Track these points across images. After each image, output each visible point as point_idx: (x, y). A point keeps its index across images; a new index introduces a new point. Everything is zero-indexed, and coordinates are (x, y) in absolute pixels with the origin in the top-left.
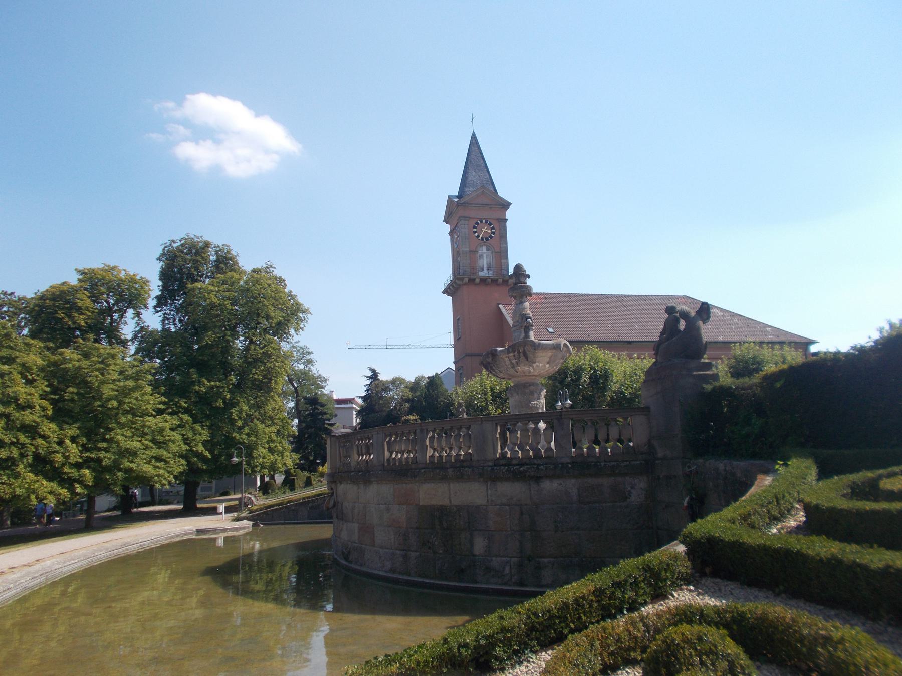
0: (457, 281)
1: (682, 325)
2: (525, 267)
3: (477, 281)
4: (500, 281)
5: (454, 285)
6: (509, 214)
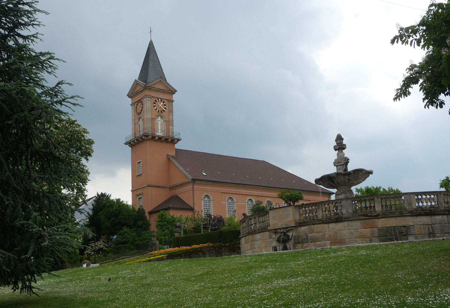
3: (157, 138)
6: (175, 97)
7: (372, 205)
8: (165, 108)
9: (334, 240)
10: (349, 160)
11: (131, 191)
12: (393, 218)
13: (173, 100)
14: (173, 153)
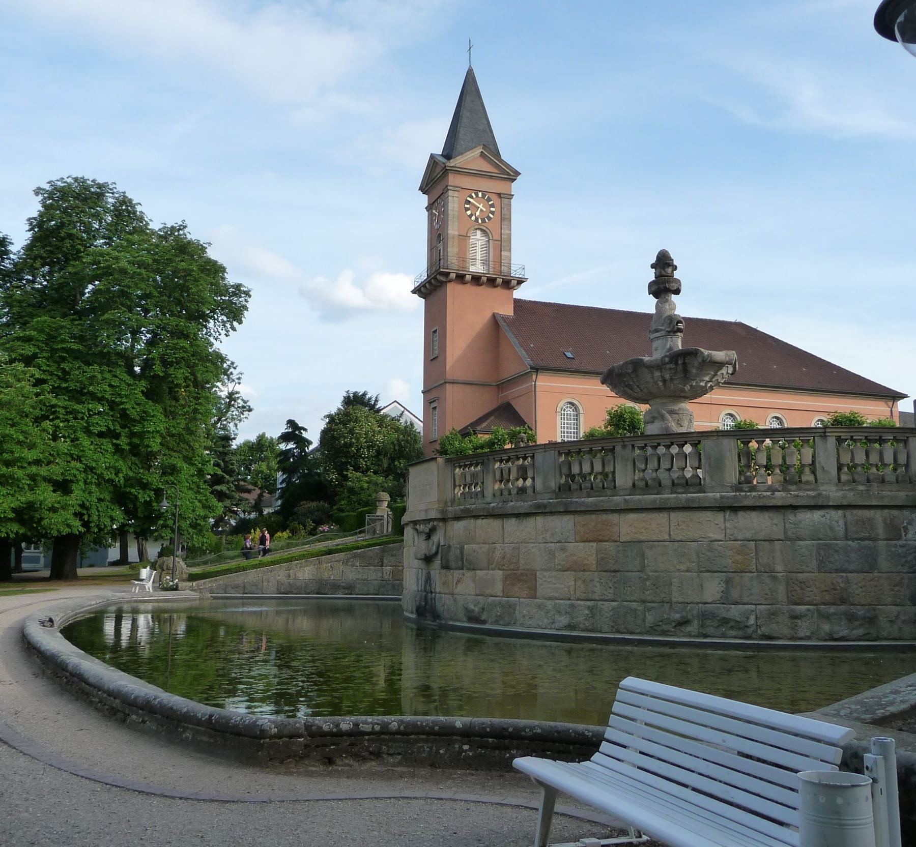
0: (438, 277)
3: (468, 277)
4: (499, 281)
5: (433, 281)
8: (493, 213)
9: (511, 570)
13: (512, 193)
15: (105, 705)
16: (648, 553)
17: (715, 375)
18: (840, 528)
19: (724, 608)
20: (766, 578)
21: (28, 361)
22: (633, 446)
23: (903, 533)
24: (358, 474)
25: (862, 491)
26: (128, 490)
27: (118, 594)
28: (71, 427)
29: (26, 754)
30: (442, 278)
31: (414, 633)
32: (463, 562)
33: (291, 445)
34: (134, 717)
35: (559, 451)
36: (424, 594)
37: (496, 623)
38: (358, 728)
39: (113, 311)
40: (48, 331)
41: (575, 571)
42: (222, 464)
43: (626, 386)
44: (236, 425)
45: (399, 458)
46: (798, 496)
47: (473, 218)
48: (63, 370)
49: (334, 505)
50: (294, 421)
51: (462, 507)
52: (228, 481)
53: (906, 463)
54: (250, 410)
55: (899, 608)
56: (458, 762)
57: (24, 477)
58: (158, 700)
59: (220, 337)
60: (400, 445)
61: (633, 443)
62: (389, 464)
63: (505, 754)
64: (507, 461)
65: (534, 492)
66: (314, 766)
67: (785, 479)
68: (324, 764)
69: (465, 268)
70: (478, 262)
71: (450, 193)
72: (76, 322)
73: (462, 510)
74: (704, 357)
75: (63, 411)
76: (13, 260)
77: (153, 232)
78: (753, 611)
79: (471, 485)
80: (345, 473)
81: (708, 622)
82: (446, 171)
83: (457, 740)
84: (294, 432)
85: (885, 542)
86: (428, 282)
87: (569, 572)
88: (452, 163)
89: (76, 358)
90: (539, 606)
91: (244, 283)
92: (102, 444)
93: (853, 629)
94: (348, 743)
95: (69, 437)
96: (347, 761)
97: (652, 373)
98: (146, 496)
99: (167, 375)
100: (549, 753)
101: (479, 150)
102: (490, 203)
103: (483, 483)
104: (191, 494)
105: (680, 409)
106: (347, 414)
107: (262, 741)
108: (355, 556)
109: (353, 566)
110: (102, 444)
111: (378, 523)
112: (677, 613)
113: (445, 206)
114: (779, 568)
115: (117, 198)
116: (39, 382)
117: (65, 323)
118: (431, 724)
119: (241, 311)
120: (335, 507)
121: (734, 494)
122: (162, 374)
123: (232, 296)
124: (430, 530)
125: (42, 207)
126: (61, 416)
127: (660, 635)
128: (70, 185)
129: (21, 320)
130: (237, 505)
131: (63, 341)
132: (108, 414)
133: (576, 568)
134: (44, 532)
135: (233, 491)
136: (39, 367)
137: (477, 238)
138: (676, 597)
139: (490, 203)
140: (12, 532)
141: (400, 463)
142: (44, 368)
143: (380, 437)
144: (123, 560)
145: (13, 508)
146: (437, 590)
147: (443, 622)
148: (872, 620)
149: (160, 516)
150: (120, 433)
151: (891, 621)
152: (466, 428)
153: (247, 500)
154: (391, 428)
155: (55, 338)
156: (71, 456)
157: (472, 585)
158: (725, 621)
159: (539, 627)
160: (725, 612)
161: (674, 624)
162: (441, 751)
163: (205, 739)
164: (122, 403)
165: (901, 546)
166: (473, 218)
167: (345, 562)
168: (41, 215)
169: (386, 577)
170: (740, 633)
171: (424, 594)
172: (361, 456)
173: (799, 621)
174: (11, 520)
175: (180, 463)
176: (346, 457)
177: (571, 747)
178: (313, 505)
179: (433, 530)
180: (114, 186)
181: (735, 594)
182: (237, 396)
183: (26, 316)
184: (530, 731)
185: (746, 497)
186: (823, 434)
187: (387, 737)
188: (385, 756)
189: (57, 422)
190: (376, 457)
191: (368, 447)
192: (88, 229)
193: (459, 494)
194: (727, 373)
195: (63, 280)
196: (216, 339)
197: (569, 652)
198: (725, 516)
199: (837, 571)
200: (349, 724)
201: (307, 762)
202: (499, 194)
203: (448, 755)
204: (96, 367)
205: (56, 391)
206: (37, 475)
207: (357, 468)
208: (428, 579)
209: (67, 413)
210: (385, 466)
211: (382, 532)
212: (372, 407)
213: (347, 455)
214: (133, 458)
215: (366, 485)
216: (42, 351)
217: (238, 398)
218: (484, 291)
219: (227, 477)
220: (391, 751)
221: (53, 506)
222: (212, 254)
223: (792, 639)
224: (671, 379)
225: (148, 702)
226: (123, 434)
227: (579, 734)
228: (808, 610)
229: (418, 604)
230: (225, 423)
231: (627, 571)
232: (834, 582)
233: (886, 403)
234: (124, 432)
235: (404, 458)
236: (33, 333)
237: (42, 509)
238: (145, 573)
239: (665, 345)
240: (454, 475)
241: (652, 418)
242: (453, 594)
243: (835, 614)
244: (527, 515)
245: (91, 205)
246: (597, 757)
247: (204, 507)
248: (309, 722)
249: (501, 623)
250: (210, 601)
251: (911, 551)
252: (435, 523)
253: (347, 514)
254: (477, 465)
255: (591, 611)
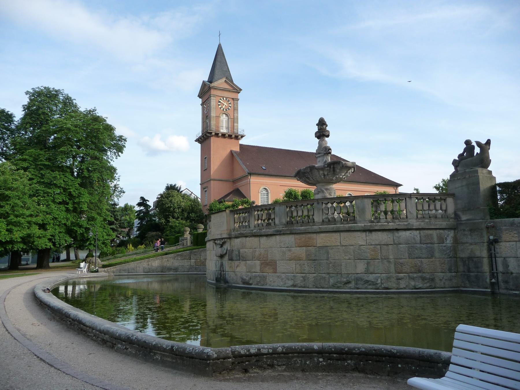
0: (207, 134)
1: (477, 150)
2: (326, 120)
3: (220, 135)
4: (233, 136)
7: (310, 214)
8: (230, 107)
9: (264, 260)
10: (330, 149)
11: (200, 184)
12: (336, 234)
14: (237, 149)
15: (98, 338)
16: (330, 251)
17: (347, 172)
18: (418, 239)
19: (366, 275)
20: (385, 261)
21: (25, 169)
22: (322, 203)
23: (445, 241)
24: (174, 220)
25: (427, 222)
26: (73, 228)
27: (71, 275)
28: (46, 200)
29: (67, 374)
30: (209, 135)
31: (215, 290)
32: (240, 257)
33: (142, 208)
34: (119, 346)
35: (287, 206)
36: (220, 272)
37: (257, 284)
38: (260, 352)
39: (64, 147)
40: (34, 156)
41: (295, 260)
42: (113, 216)
43: (307, 178)
44: (118, 199)
45: (191, 213)
46: (399, 225)
47: (222, 109)
48: (41, 174)
49: (164, 233)
50: (143, 197)
51: (239, 232)
52: (116, 224)
53: (445, 209)
54: (124, 192)
55: (444, 274)
56: (317, 368)
57: (25, 222)
58: (134, 337)
59: (113, 159)
60: (192, 207)
61: (322, 201)
62: (188, 216)
63: (344, 363)
64: (261, 211)
65: (275, 224)
66: (238, 374)
67: (393, 217)
68: (243, 373)
69: (218, 130)
70: (224, 128)
71: (212, 98)
72: (47, 152)
73: (239, 234)
74: (343, 165)
75: (42, 192)
76: (16, 124)
77: (81, 113)
78: (379, 277)
79: (243, 222)
80: (168, 219)
81: (359, 282)
82: (210, 88)
83: (315, 356)
84: (143, 202)
85: (438, 245)
86: (202, 137)
87: (292, 261)
88: (212, 85)
89: (47, 169)
90: (278, 277)
91: (123, 135)
92: (60, 207)
93: (424, 284)
94: (255, 360)
95: (45, 204)
96: (255, 371)
97: (319, 172)
98: (81, 231)
99: (90, 176)
100: (370, 362)
101: (224, 79)
102: (229, 102)
103: (249, 221)
104: (101, 229)
105: (330, 188)
106: (168, 194)
107: (208, 362)
108: (178, 255)
109: (177, 260)
110: (60, 207)
111: (185, 241)
112: (345, 278)
113: (210, 103)
114: (391, 257)
115: (64, 97)
116: (30, 179)
117: (42, 152)
118: (300, 348)
119: (122, 148)
120: (164, 234)
121: (370, 224)
122: (87, 176)
123: (118, 141)
124: (223, 243)
125: (29, 100)
126: (41, 195)
127: (336, 288)
128: (42, 90)
129: (21, 151)
130: (120, 234)
131: (41, 161)
132: (62, 194)
133: (297, 259)
134: (35, 247)
135: (118, 228)
136: (30, 172)
137: (224, 118)
138: (344, 271)
139: (229, 102)
140: (20, 247)
141: (192, 215)
142: (33, 173)
143: (183, 204)
144: (68, 259)
145: (20, 237)
146: (227, 270)
147: (230, 284)
148: (433, 280)
149: (88, 239)
150: (68, 202)
151: (441, 280)
152: (221, 199)
153: (124, 232)
154: (188, 200)
155: (38, 159)
156: (47, 212)
157: (245, 267)
158: (367, 282)
159: (278, 286)
160: (366, 277)
161: (343, 284)
162: (308, 363)
163: (169, 359)
164: (69, 189)
165: (444, 246)
166: (222, 109)
167: (174, 258)
168: (29, 103)
169: (192, 264)
170: (374, 287)
171: (220, 272)
172: (175, 212)
173: (400, 281)
174: (19, 242)
175: (96, 216)
176: (168, 212)
177: (384, 359)
178: (154, 233)
179: (224, 243)
180: (63, 91)
181: (371, 269)
182: (118, 186)
183: (23, 150)
184: (358, 350)
185: (376, 225)
186: (410, 197)
187: (276, 356)
188: (276, 366)
189: (39, 198)
190: (182, 212)
191: (178, 208)
192: (51, 110)
193: (237, 226)
194: (351, 172)
195: (40, 133)
196: (111, 160)
197: (293, 297)
198: (366, 234)
199: (417, 258)
200: (255, 349)
201: (233, 372)
202: (233, 99)
203: (311, 364)
204: (57, 172)
205: (39, 183)
206: (31, 221)
207: (173, 217)
208: (222, 265)
209: (44, 193)
210: (186, 216)
211: (187, 245)
212: (178, 191)
213: (169, 211)
214: (75, 214)
215: (178, 225)
216: (31, 165)
217: (118, 187)
218: (227, 140)
219: (115, 222)
220: (280, 364)
221: (39, 236)
222: (109, 122)
223: (398, 289)
224: (328, 174)
225: (129, 338)
226: (70, 203)
227: (389, 351)
228: (405, 276)
229: (216, 276)
230: (112, 198)
231: (320, 260)
232: (416, 262)
233: (394, 188)
234: (71, 202)
235: (194, 213)
236: (27, 157)
237: (34, 237)
238: (82, 265)
239: (323, 159)
240: (234, 218)
241: (318, 192)
242: (234, 272)
243: (416, 277)
244: (271, 235)
245: (52, 99)
246: (448, 374)
247: (107, 235)
248: (233, 349)
249: (259, 284)
250: (113, 277)
251: (449, 248)
252: (226, 240)
253: (170, 237)
254: (246, 213)
255: (304, 278)
